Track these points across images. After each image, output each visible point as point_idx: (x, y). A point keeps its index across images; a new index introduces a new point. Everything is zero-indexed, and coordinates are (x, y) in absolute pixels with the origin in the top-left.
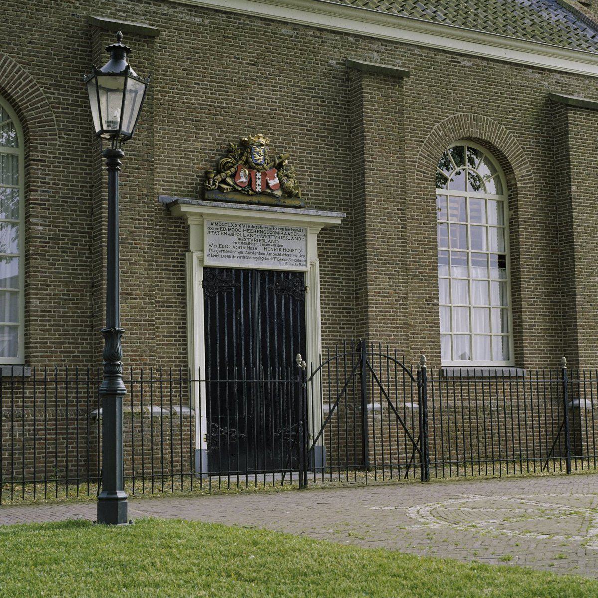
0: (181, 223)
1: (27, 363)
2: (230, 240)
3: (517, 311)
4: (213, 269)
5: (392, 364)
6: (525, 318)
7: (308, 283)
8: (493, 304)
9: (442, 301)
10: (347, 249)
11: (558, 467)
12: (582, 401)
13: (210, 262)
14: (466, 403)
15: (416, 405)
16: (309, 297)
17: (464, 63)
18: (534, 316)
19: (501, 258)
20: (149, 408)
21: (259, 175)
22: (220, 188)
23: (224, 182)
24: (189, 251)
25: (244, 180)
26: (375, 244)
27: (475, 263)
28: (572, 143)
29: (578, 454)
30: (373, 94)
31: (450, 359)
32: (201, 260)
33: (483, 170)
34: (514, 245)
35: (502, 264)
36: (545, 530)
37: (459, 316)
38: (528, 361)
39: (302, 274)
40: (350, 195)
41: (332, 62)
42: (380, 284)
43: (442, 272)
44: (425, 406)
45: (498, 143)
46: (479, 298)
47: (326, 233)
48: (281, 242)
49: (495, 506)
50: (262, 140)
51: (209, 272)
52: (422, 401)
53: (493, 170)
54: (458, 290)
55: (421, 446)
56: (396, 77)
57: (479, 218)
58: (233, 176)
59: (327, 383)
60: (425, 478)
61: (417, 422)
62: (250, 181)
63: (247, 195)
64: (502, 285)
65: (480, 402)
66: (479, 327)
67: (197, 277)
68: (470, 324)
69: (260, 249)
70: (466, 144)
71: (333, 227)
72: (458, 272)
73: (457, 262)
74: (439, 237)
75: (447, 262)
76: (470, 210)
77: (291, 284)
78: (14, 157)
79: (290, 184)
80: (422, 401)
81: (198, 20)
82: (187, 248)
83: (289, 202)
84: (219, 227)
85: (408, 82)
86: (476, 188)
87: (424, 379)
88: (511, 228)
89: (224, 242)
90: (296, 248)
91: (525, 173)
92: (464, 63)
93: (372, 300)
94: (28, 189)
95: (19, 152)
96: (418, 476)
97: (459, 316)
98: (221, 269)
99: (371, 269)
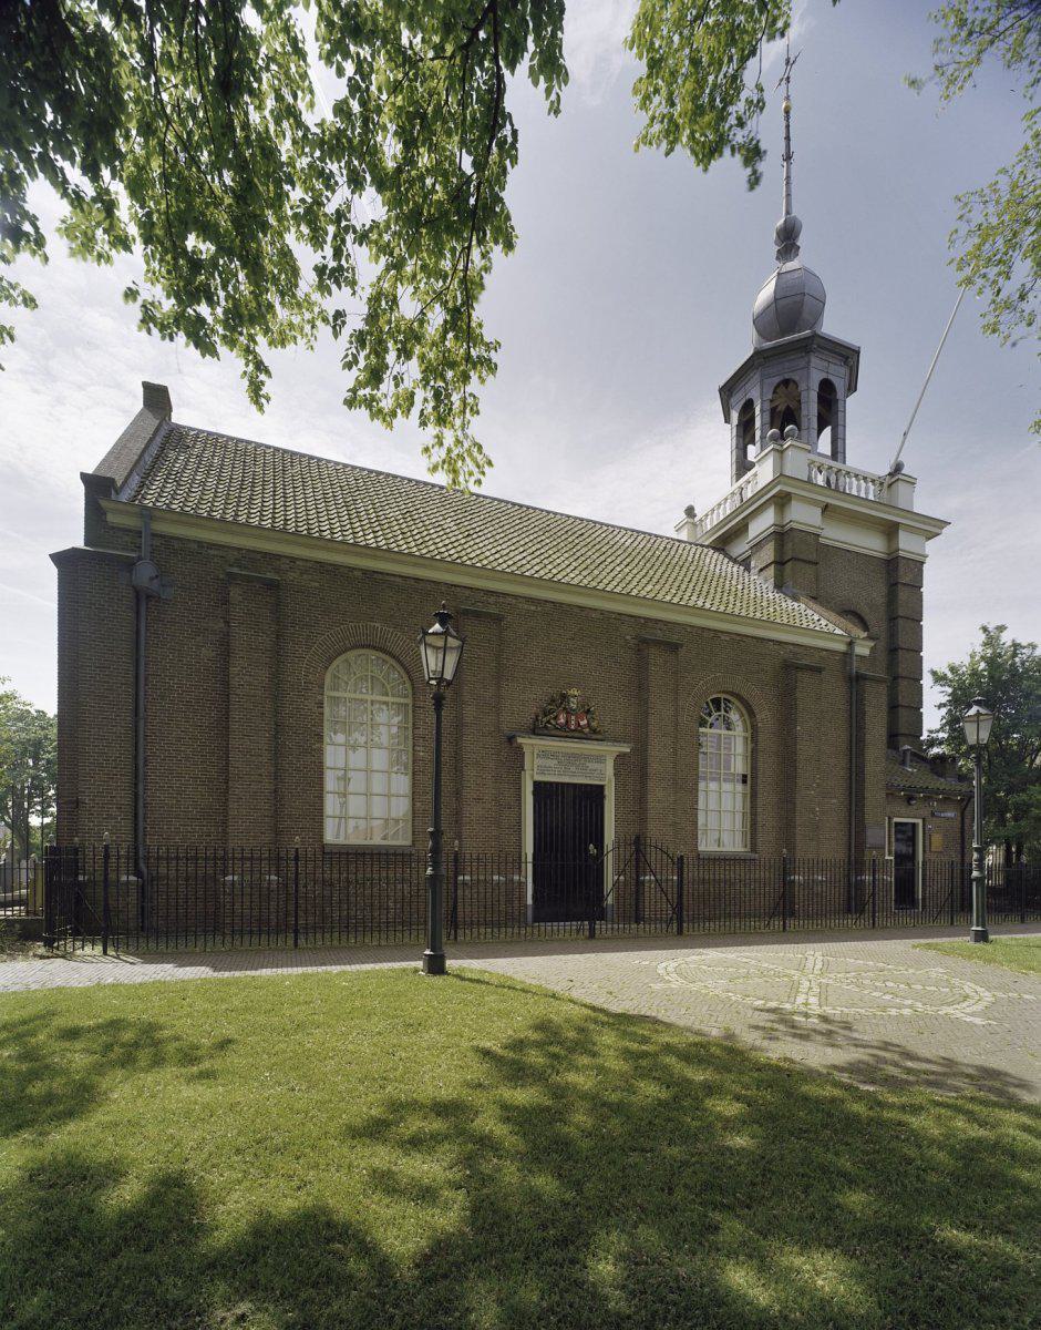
0: (519, 753)
1: (414, 844)
2: (552, 763)
3: (754, 814)
4: (540, 783)
5: (665, 856)
6: (759, 819)
7: (606, 793)
8: (737, 808)
9: (701, 805)
10: (634, 770)
11: (777, 923)
12: (797, 877)
13: (538, 778)
14: (482, 878)
15: (675, 878)
16: (606, 803)
17: (723, 638)
18: (768, 819)
19: (745, 776)
20: (267, 877)
21: (573, 718)
22: (546, 727)
23: (548, 722)
24: (523, 770)
25: (562, 721)
26: (654, 767)
27: (725, 780)
28: (798, 695)
29: (792, 914)
30: (656, 657)
31: (706, 845)
32: (533, 777)
33: (734, 716)
34: (754, 768)
35: (744, 782)
36: (761, 994)
37: (712, 817)
38: (760, 847)
39: (602, 787)
40: (640, 740)
41: (628, 637)
42: (658, 795)
43: (702, 785)
44: (682, 878)
45: (744, 694)
46: (727, 804)
47: (620, 759)
48: (588, 764)
49: (725, 964)
50: (576, 693)
51: (537, 785)
52: (680, 875)
53: (742, 715)
54: (713, 798)
55: (679, 909)
56: (674, 648)
57: (730, 749)
58: (556, 718)
59: (617, 860)
60: (680, 932)
61: (675, 896)
62: (567, 722)
63: (565, 732)
64: (744, 795)
65: (722, 876)
66: (726, 825)
67: (528, 789)
68: (721, 819)
69: (573, 769)
70: (723, 696)
71: (625, 754)
72: (713, 786)
73: (713, 779)
74: (701, 762)
75: (705, 779)
76: (728, 747)
77: (596, 793)
78: (407, 705)
79: (594, 724)
80: (680, 875)
81: (533, 608)
82: (522, 768)
83: (594, 736)
84: (544, 754)
85: (682, 652)
86: (728, 729)
87: (682, 863)
88: (754, 756)
89: (545, 760)
90: (597, 764)
91: (765, 716)
92: (723, 638)
93: (651, 805)
94: (415, 727)
95: (409, 701)
96: (675, 929)
97: (712, 817)
98: (546, 783)
99: (650, 784)
